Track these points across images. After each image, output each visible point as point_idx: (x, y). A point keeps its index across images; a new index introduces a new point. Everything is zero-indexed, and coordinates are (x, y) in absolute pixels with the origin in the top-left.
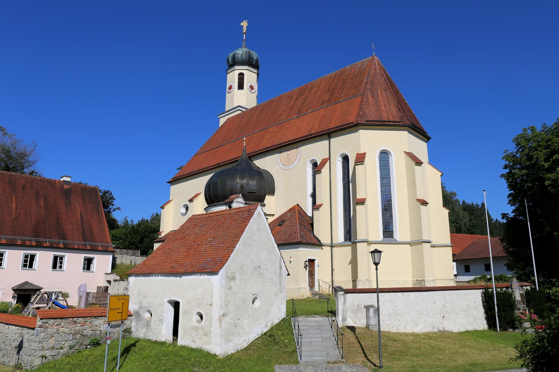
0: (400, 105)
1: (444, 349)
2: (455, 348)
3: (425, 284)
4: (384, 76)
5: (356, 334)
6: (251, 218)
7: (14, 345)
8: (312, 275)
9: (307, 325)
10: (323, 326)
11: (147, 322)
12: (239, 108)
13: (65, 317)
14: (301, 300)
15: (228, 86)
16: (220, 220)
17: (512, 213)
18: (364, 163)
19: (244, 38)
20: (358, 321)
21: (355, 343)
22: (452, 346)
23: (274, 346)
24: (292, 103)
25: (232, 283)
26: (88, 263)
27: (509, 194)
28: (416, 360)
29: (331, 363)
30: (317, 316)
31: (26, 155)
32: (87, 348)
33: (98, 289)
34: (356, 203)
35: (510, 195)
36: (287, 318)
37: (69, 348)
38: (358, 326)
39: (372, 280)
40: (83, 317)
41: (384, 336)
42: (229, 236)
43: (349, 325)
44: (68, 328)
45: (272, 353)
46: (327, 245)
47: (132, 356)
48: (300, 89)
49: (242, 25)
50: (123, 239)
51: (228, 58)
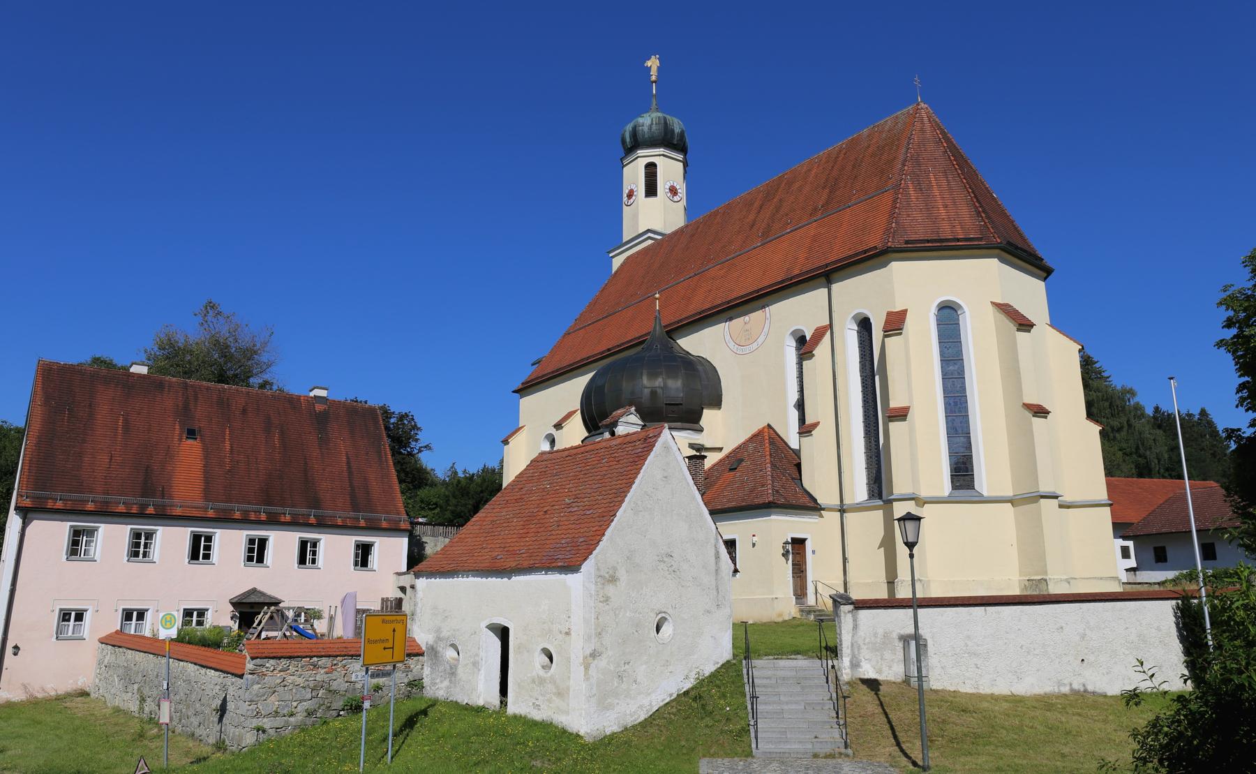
0: (979, 203)
1: (1077, 732)
2: (1103, 730)
3: (1048, 588)
4: (942, 143)
5: (880, 696)
6: (649, 454)
7: (214, 706)
8: (799, 570)
9: (774, 675)
10: (810, 679)
11: (451, 668)
12: (650, 235)
13: (296, 654)
14: (778, 623)
15: (626, 192)
16: (589, 460)
17: (1248, 427)
18: (904, 332)
19: (654, 92)
20: (885, 669)
21: (877, 715)
22: (1100, 725)
23: (702, 718)
24: (752, 217)
25: (610, 590)
26: (363, 555)
27: (1240, 385)
28: (1008, 756)
29: (822, 758)
30: (799, 656)
31: (255, 352)
32: (339, 715)
33: (382, 603)
34: (889, 417)
35: (1242, 387)
36: (734, 662)
37: (305, 714)
38: (885, 679)
39: (929, 581)
40: (329, 656)
41: (942, 701)
42: (604, 493)
43: (866, 677)
44: (303, 676)
45: (697, 733)
46: (831, 508)
47: (418, 735)
48: (768, 184)
49: (649, 66)
50: (441, 507)
51: (623, 135)
